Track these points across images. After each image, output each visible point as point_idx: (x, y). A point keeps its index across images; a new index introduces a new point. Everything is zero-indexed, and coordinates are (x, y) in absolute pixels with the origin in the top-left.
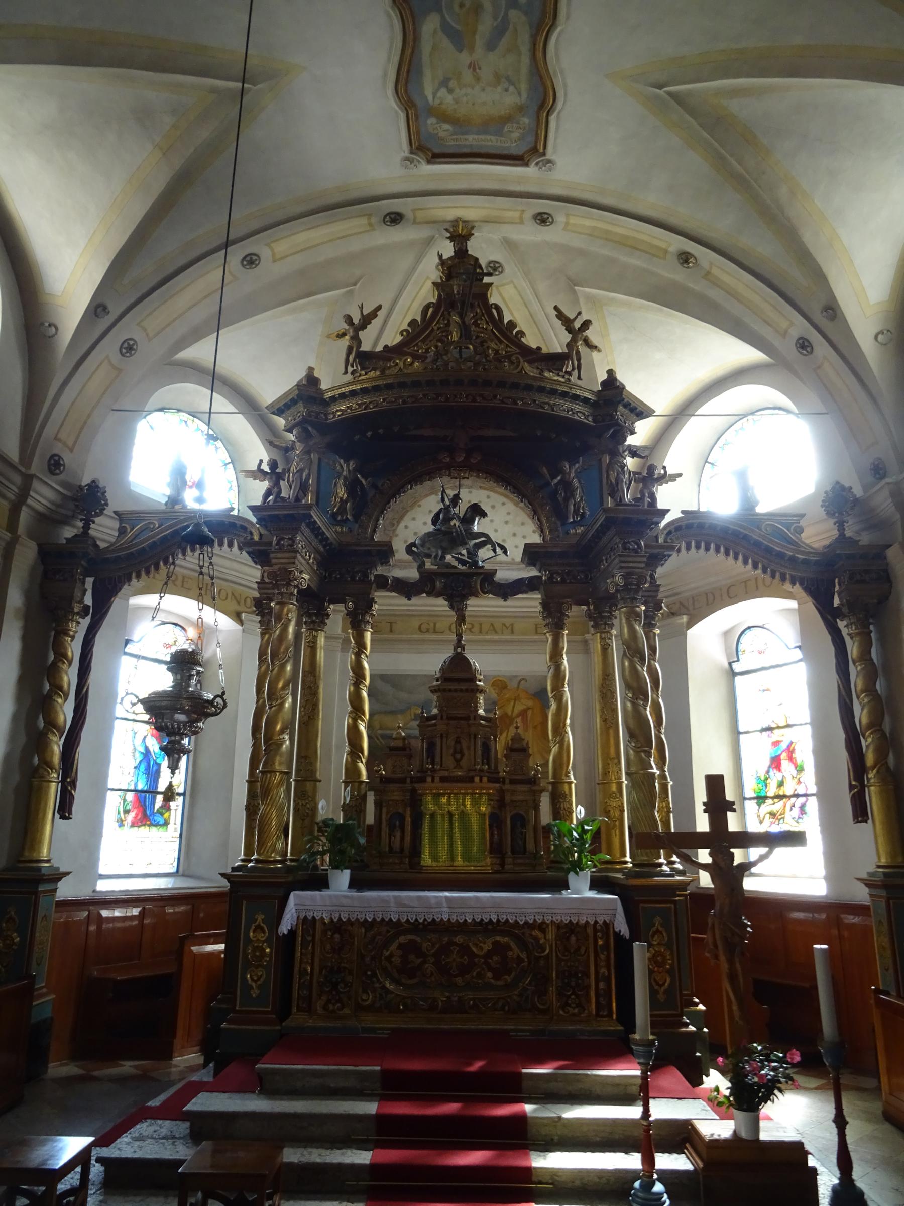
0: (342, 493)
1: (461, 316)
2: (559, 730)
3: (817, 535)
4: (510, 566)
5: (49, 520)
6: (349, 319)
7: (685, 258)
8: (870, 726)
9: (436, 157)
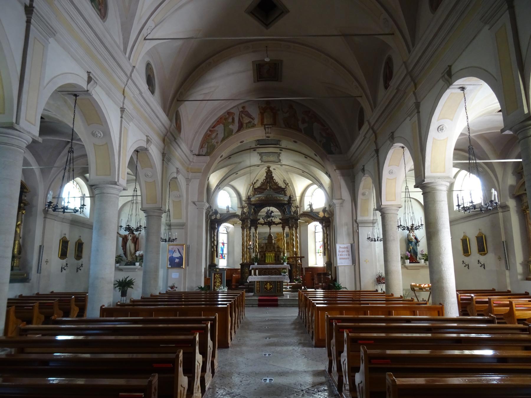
3: (321, 215)
4: (277, 220)
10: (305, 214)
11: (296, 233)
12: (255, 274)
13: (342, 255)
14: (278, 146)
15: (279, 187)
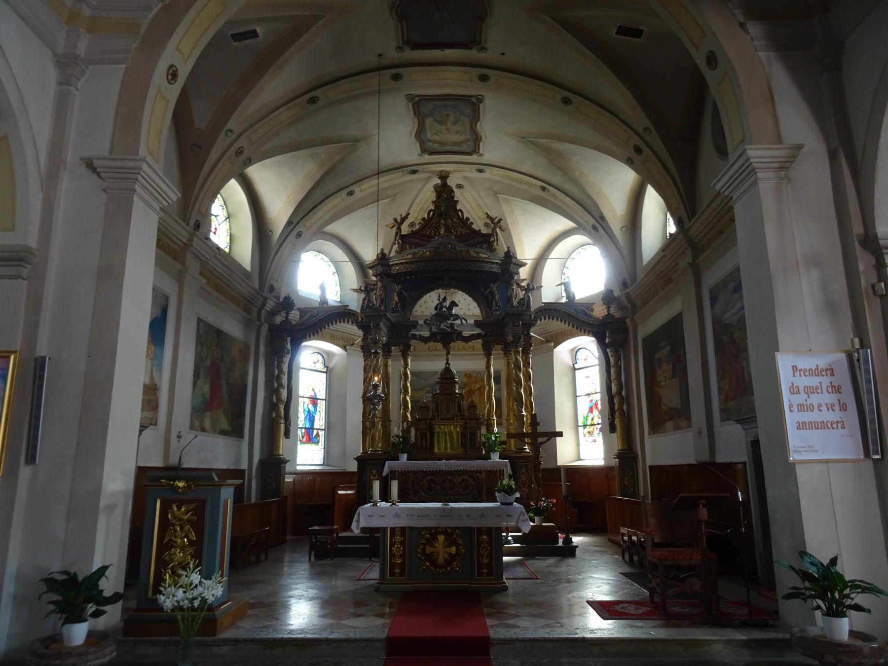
0: (396, 298)
1: (445, 220)
2: (489, 398)
3: (599, 312)
5: (273, 313)
6: (396, 220)
7: (543, 189)
8: (617, 393)
9: (432, 153)
10: (551, 310)
11: (527, 364)
12: (385, 496)
13: (811, 408)
14: (472, 54)
15: (474, 230)
